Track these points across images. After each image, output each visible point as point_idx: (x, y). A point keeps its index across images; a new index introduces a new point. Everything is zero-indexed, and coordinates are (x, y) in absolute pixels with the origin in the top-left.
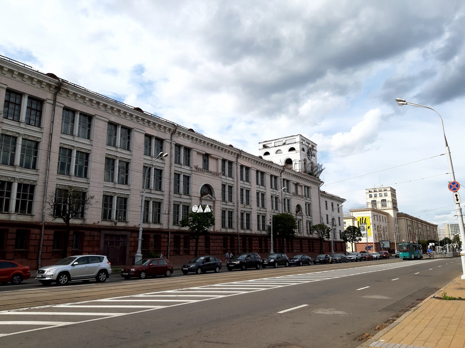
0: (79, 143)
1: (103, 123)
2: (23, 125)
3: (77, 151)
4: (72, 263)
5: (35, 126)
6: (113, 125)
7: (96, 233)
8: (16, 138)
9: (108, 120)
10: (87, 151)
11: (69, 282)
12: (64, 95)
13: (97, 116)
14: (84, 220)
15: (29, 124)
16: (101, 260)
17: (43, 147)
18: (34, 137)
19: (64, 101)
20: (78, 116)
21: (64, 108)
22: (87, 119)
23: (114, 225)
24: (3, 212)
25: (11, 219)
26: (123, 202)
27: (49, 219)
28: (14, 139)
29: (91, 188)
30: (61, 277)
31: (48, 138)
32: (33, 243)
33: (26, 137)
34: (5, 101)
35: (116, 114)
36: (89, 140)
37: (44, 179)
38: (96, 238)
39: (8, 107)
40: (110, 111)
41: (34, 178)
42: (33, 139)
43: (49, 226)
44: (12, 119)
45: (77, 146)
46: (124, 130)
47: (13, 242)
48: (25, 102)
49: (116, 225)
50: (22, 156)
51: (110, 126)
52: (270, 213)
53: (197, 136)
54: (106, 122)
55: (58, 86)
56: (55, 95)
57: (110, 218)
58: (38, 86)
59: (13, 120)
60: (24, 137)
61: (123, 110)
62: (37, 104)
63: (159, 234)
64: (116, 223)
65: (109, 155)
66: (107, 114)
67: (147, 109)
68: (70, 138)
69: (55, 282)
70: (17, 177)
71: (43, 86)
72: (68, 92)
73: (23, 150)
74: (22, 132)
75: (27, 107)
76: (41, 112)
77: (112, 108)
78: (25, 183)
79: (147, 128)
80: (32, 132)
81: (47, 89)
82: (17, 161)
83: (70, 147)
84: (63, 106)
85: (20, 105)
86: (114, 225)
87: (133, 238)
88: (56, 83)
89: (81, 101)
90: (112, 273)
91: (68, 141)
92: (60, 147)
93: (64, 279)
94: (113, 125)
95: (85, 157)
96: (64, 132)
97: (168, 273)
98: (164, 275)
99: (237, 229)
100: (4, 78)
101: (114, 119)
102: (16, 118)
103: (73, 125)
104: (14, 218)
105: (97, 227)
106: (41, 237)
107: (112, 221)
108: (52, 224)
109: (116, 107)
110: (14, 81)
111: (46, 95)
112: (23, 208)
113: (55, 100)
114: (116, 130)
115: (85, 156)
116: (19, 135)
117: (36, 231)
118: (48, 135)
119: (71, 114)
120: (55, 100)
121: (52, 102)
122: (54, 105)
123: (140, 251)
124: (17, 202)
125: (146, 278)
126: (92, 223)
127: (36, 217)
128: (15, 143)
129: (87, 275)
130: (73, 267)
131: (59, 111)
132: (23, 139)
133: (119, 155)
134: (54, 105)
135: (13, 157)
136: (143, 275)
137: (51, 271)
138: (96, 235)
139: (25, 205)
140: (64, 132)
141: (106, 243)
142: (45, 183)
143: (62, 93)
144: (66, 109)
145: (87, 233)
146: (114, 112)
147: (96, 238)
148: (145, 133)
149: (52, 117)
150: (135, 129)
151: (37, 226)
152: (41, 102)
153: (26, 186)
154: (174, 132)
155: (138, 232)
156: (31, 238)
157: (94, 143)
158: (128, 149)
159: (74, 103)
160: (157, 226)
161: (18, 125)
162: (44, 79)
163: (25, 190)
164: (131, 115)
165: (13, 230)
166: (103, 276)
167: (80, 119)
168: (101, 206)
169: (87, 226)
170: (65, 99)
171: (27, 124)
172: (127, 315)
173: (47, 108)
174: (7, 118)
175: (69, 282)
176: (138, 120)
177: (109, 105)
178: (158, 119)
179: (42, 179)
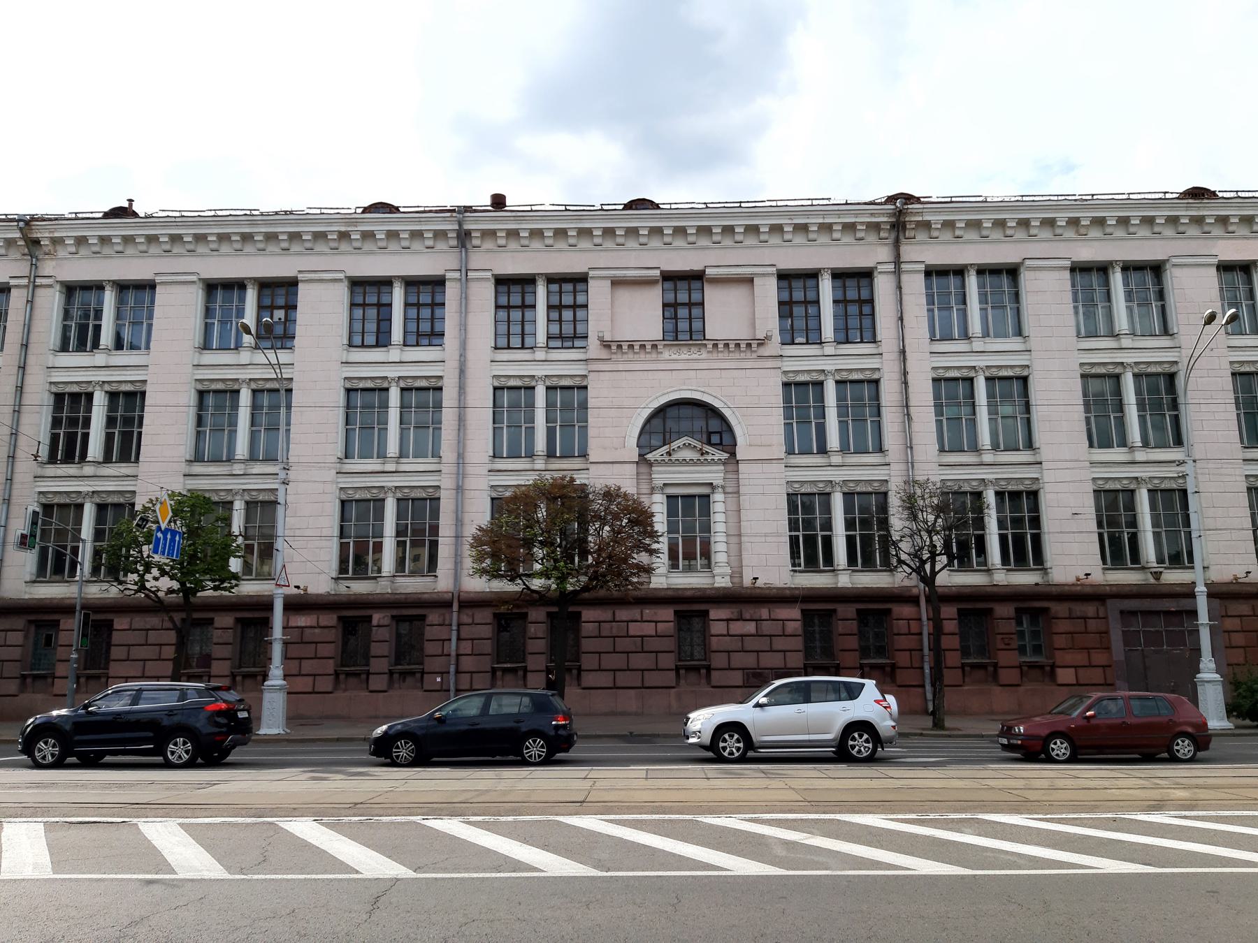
0: (988, 353)
1: (1056, 274)
2: (829, 350)
3: (987, 379)
4: (754, 701)
5: (862, 342)
6: (1089, 274)
7: (1090, 609)
8: (971, 380)
9: (1068, 263)
10: (1018, 372)
11: (750, 754)
12: (921, 236)
13: (1028, 262)
14: (1045, 571)
15: (847, 342)
16: (853, 692)
17: (889, 393)
18: (1012, 367)
19: (924, 252)
20: (1117, 278)
21: (1073, 270)
22: (1149, 277)
23: (1152, 581)
24: (1130, 565)
25: (840, 585)
26: (1174, 503)
27: (477, 585)
28: (967, 384)
29: (1048, 476)
30: (736, 736)
31: (897, 363)
32: (903, 642)
33: (845, 376)
34: (781, 303)
35: (1095, 233)
36: (1019, 339)
37: (904, 473)
38: (1093, 625)
39: (791, 315)
40: (1070, 234)
41: (879, 474)
42: (1102, 370)
43: (471, 603)
44: (804, 340)
45: (983, 364)
46: (1134, 277)
47: (853, 642)
48: (826, 287)
49: (1158, 579)
50: (843, 425)
51: (1229, 276)
52: (472, 478)
53: (411, 221)
54: (1064, 268)
55: (900, 216)
56: (897, 244)
57: (1136, 557)
58: (848, 239)
59: (807, 343)
60: (838, 378)
61: (1111, 215)
62: (855, 281)
63: (411, 614)
64: (1157, 575)
65: (1242, 363)
66: (1063, 244)
67: (676, 192)
68: (961, 346)
69: (713, 752)
70: (838, 479)
71: (859, 235)
72: (927, 225)
73: (1141, 405)
74: (829, 365)
75: (834, 302)
76: (871, 301)
77: (1074, 222)
78: (1010, 488)
79: (1221, 242)
80: (855, 359)
81: (872, 238)
82: (833, 441)
83: (965, 373)
84: (922, 267)
85: (817, 302)
86: (1152, 581)
87: (1237, 621)
88: (890, 215)
89: (972, 235)
90: (902, 735)
91: (956, 357)
92: (1233, 374)
93: (735, 747)
94: (1089, 274)
95: (1014, 387)
96: (941, 334)
97: (1184, 747)
98: (1165, 755)
99: (389, 577)
100: (767, 251)
101: (1089, 252)
102: (812, 336)
103: (965, 311)
104: (845, 580)
105: (344, 599)
106: (921, 626)
107: (1143, 568)
108: (946, 590)
109: (1086, 216)
110: (602, 254)
111: (873, 254)
112: (689, 556)
113: (897, 261)
114: (1107, 283)
115: (1016, 386)
116: (976, 371)
117: (906, 610)
118: (895, 356)
119: (1095, 278)
120: (897, 261)
121: (891, 267)
122: (898, 272)
123: (1213, 665)
124: (850, 541)
125: (190, 765)
126: (1071, 579)
127: (443, 582)
128: (821, 398)
129: (806, 737)
130: (760, 715)
131: (915, 284)
132: (837, 382)
133: (980, 361)
134: (898, 272)
135: (821, 430)
136: (1060, 748)
137: (703, 720)
138: (1090, 615)
139: (1025, 546)
140: (941, 334)
141: (1129, 638)
142: (459, 489)
143: (911, 234)
144: (932, 272)
145: (1058, 608)
146: (1083, 231)
147: (1093, 625)
148: (1215, 261)
149: (902, 305)
150: (1175, 260)
151: (442, 604)
152: (866, 275)
153: (1015, 495)
154: (464, 237)
155: (1192, 595)
156: (896, 631)
157: (1033, 343)
158: (1166, 331)
159: (954, 247)
160: (1025, 579)
161: (818, 352)
162: (856, 216)
163: (688, 511)
164: (104, 240)
165: (848, 611)
166: (732, 744)
167: (1126, 284)
168: (1093, 525)
169: (1054, 589)
170: (925, 247)
171: (839, 343)
172: (963, 877)
173: (883, 286)
174: (793, 343)
175: (750, 754)
176: (1181, 229)
177: (1062, 217)
178: (755, 210)
179: (899, 473)
